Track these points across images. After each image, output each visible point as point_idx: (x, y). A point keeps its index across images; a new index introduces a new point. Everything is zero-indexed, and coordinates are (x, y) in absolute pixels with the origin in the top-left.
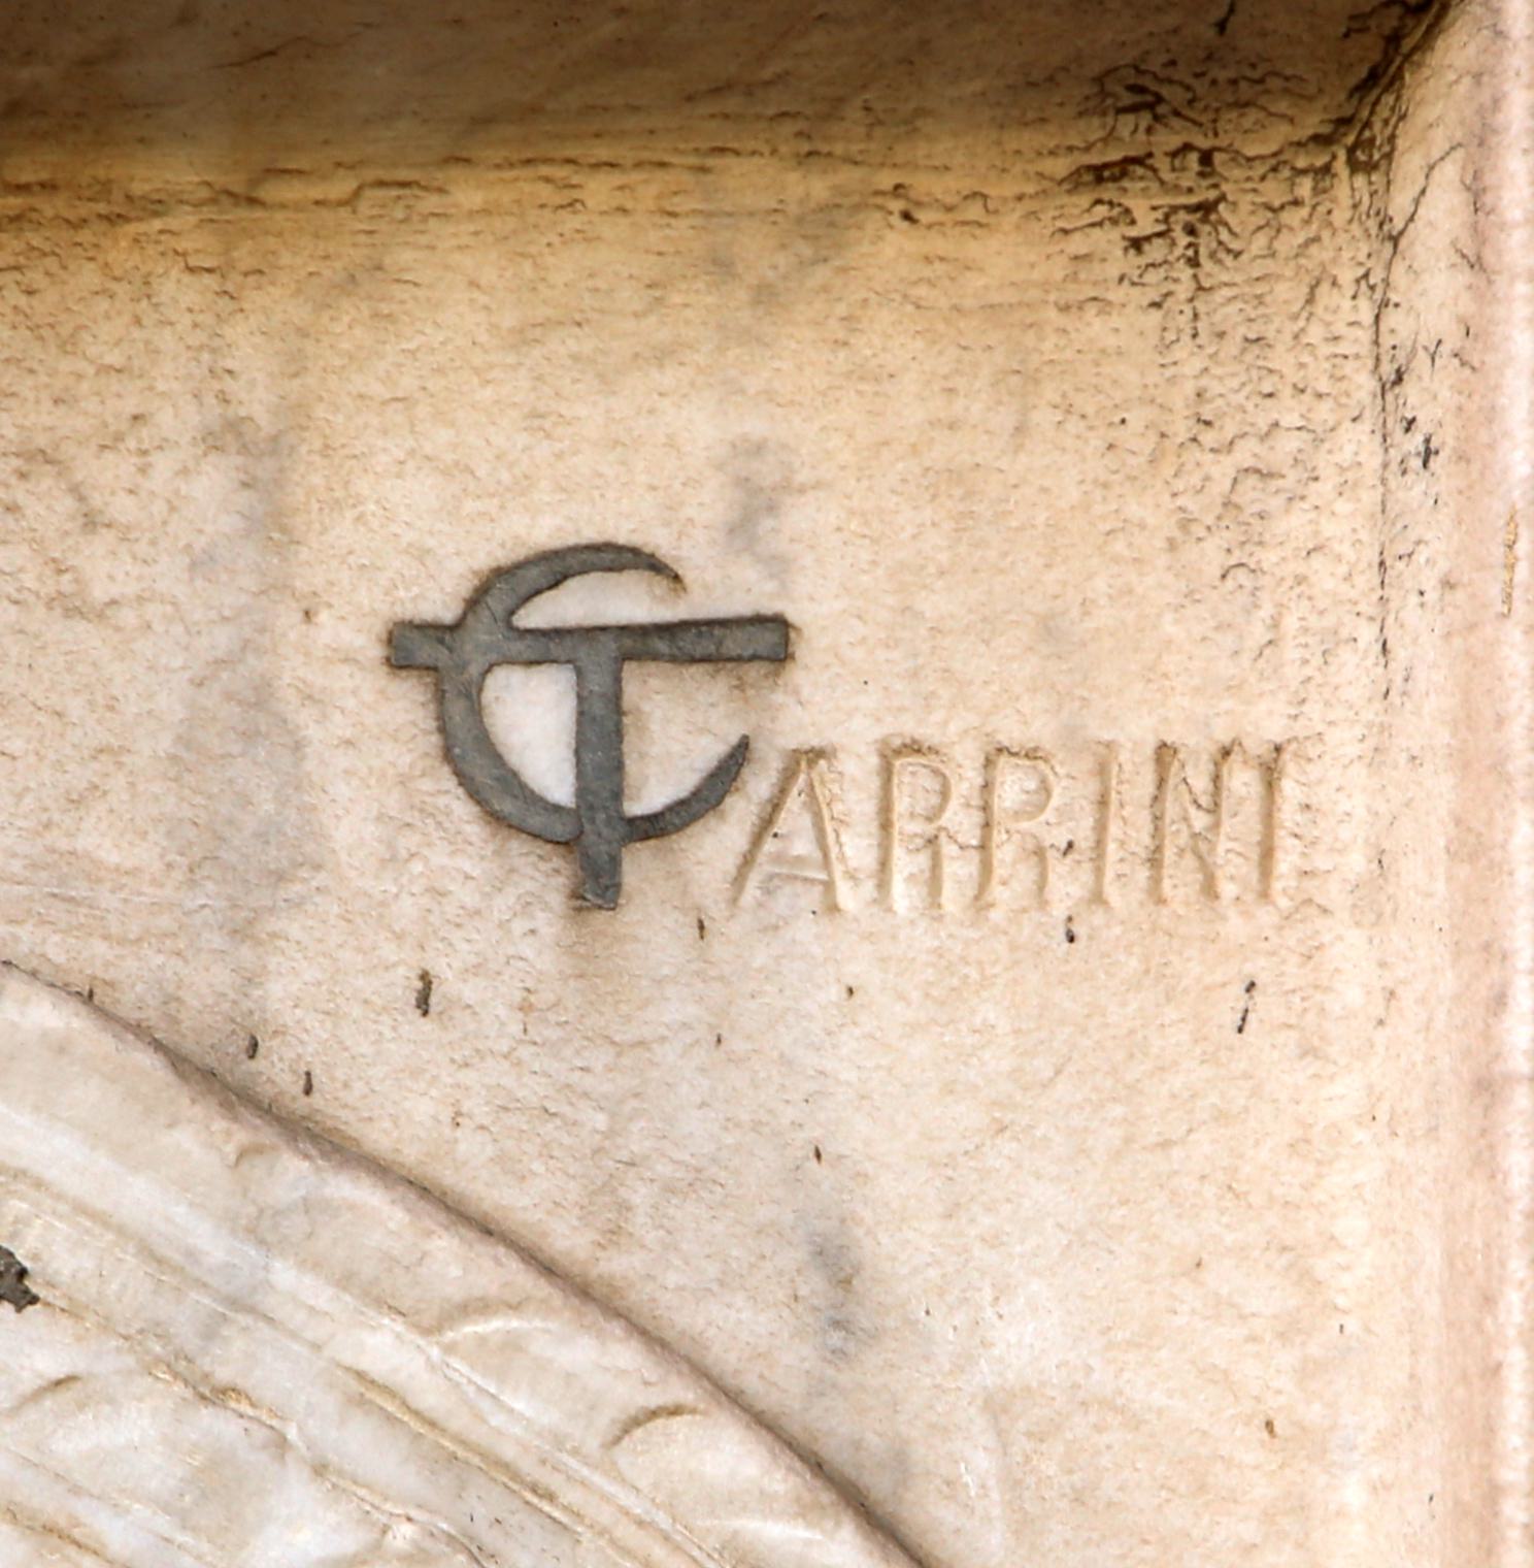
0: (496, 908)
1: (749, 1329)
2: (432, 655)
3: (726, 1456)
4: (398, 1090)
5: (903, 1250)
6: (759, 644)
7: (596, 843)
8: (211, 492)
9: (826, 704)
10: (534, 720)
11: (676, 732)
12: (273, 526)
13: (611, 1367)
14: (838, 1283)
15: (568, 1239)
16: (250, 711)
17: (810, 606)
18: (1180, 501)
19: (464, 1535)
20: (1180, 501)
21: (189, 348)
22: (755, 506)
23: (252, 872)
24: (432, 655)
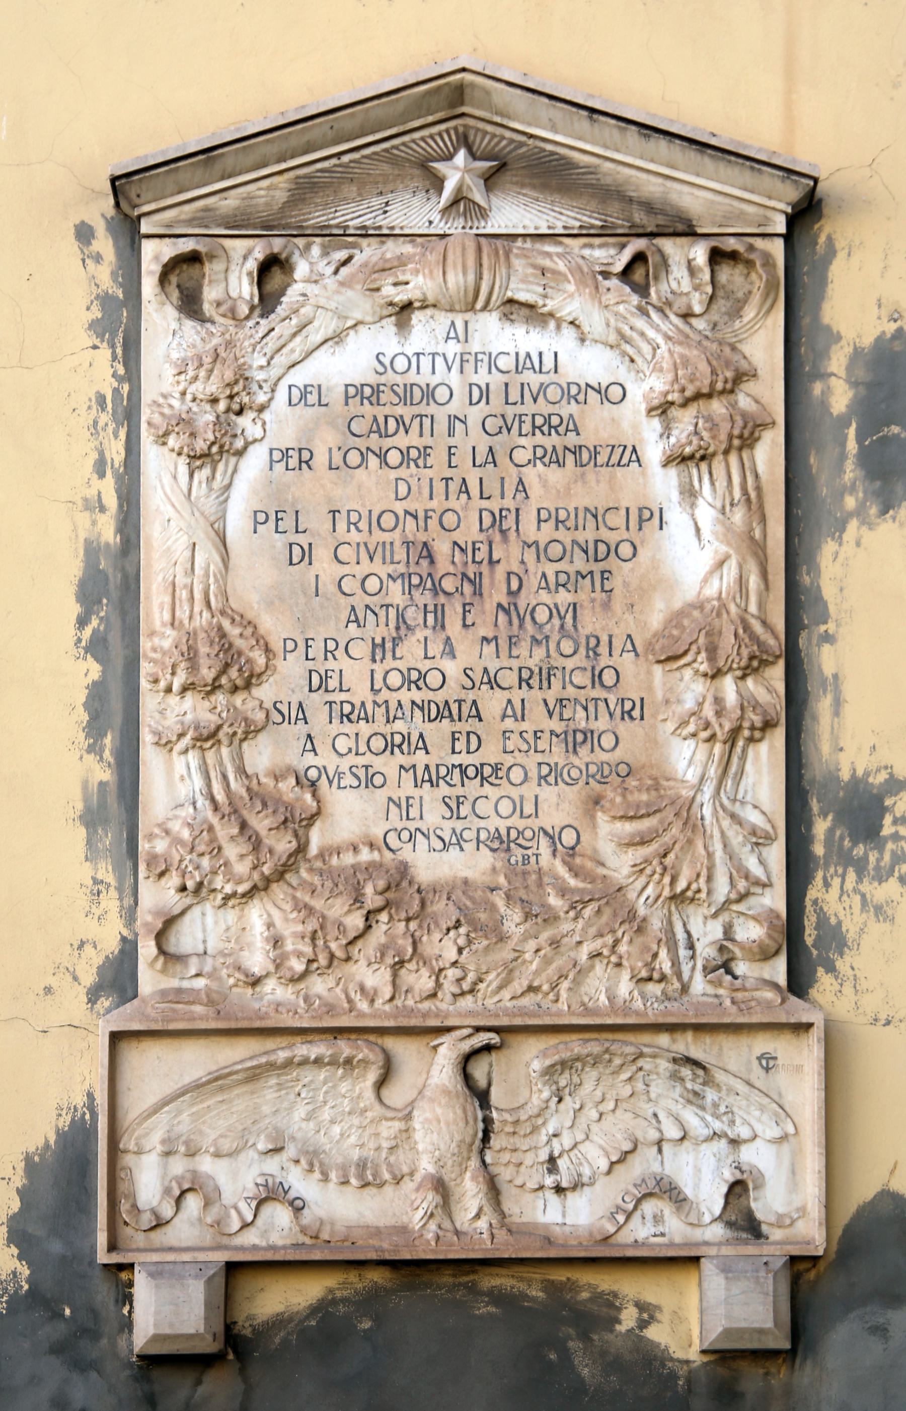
0: (762, 1073)
1: (776, 1097)
2: (759, 1059)
3: (775, 1105)
4: (757, 1084)
5: (784, 1093)
6: (775, 1058)
7: (767, 1069)
8: (747, 1049)
9: (780, 1062)
10: (764, 1062)
11: (771, 1063)
12: (750, 1051)
13: (768, 1100)
14: (780, 1094)
15: (765, 1090)
16: (749, 1062)
17: (779, 1056)
18: (176, 687)
19: (759, 170)
20: (176, 687)
21: (613, 1111)
22: (775, 1050)
23: (750, 1071)
24: (759, 1059)
